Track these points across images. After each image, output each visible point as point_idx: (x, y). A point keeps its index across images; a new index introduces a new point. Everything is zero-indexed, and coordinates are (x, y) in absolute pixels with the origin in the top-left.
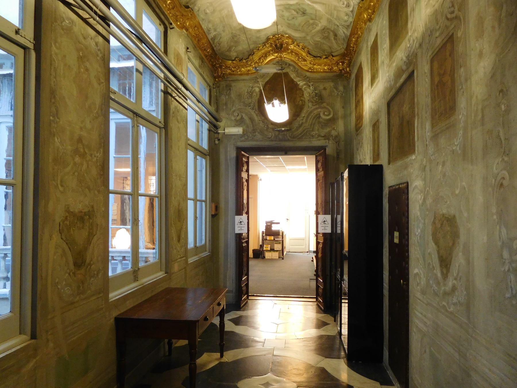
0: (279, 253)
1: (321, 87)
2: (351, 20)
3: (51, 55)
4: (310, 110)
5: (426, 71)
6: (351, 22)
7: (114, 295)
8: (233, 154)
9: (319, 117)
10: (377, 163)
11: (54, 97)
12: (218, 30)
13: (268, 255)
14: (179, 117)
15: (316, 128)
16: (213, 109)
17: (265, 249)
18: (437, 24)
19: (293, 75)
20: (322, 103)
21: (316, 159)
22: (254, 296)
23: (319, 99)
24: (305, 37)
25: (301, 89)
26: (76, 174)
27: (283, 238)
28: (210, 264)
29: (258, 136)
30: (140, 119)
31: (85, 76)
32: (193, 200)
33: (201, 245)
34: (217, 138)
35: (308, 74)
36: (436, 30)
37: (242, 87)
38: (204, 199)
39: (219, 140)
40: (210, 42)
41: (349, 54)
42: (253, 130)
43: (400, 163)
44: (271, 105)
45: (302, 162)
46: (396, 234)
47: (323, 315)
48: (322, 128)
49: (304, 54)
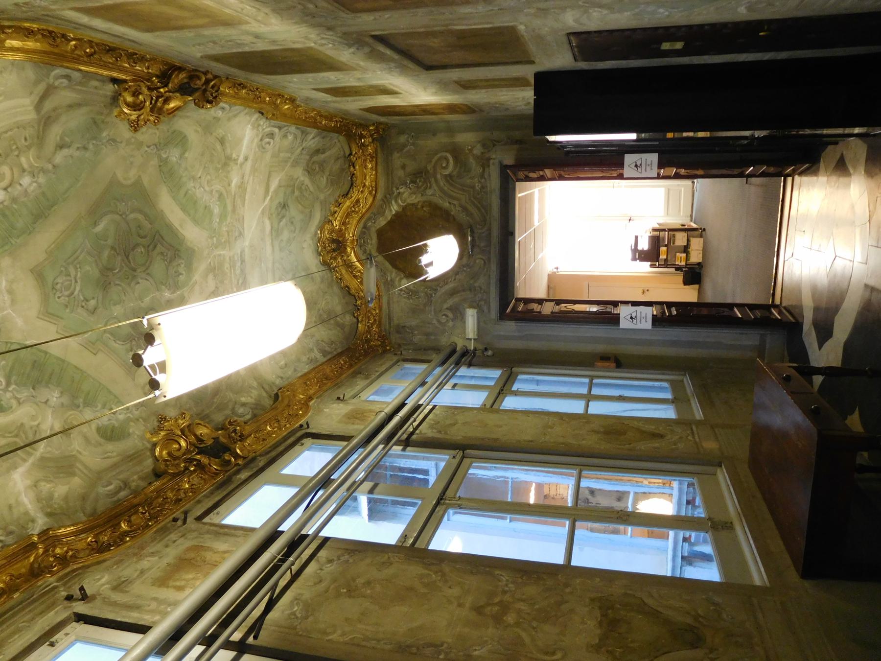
0: (693, 237)
1: (401, 173)
2: (293, 129)
3: (346, 643)
4: (438, 193)
5: (372, 18)
6: (297, 128)
7: (758, 575)
8: (510, 327)
9: (450, 176)
10: (532, 81)
11: (409, 646)
12: (311, 346)
13: (696, 257)
14: (448, 422)
15: (468, 181)
16: (437, 358)
17: (683, 263)
18: (295, 7)
19: (382, 222)
20: (427, 172)
21: (522, 180)
22: (773, 295)
23: (420, 177)
24: (321, 203)
25: (404, 208)
26: (535, 624)
27: (664, 230)
28: (704, 377)
29: (481, 281)
30: (449, 493)
31: (378, 588)
32: (589, 401)
33: (670, 389)
34: (483, 352)
35: (379, 196)
36: (305, 8)
37: (399, 309)
38: (587, 380)
39: (486, 349)
40: (330, 359)
41: (347, 128)
42: (470, 290)
43: (532, 48)
44: (429, 269)
45: (529, 199)
46: (666, 46)
47: (822, 164)
48: (469, 171)
49: (348, 203)
